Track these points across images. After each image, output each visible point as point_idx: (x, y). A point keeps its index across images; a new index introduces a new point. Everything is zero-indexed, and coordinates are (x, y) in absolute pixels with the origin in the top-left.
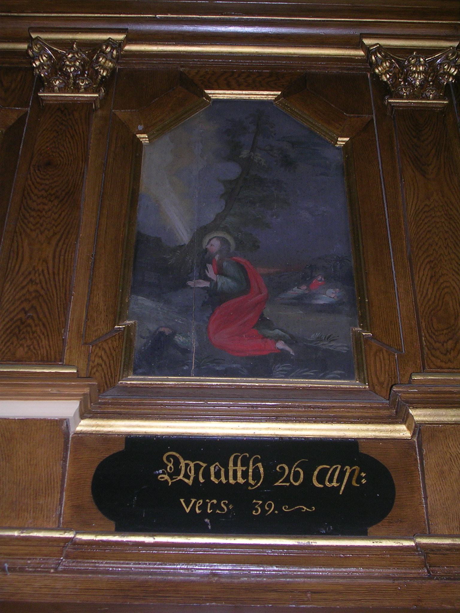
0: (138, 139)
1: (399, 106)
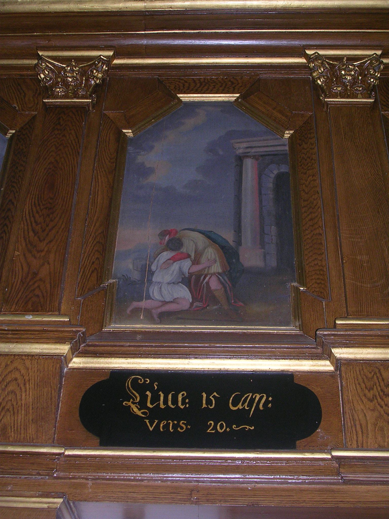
1: (336, 104)
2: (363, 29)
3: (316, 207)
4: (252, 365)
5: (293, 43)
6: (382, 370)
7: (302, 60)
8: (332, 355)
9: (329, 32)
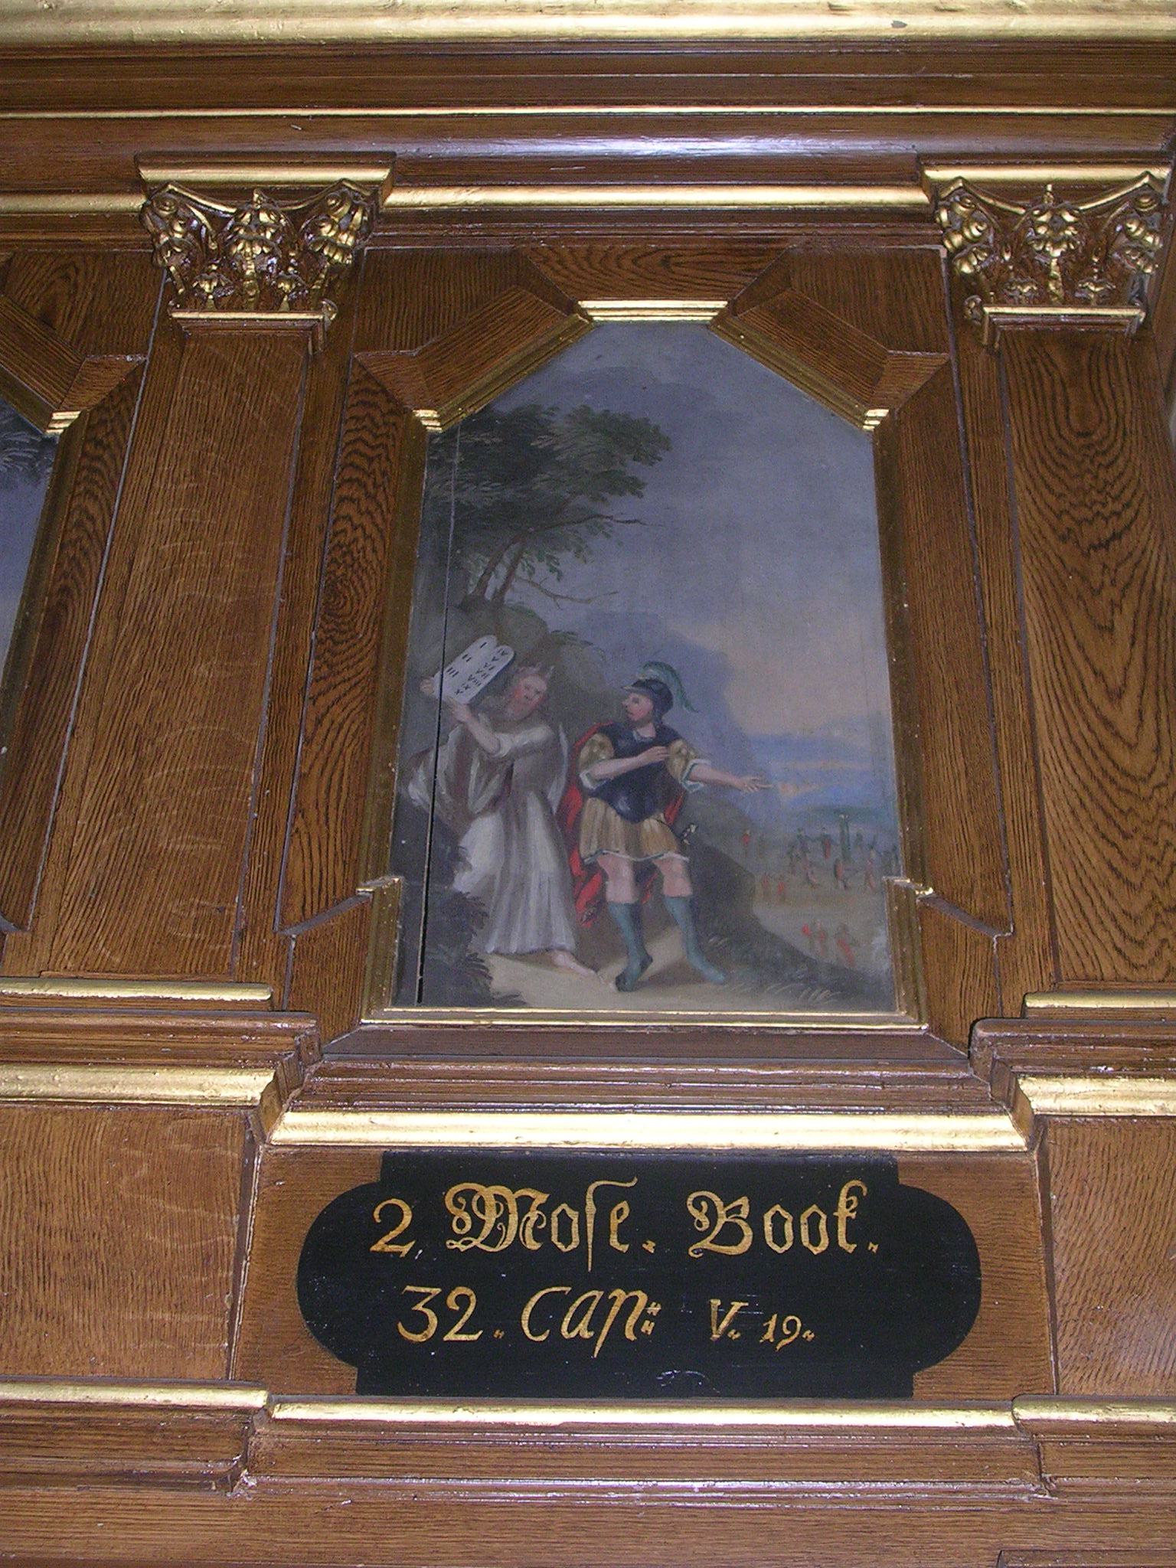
0: (418, 420)
1: (1015, 322)
5: (690, 145)
7: (919, 197)
8: (1020, 1099)
9: (549, 104)
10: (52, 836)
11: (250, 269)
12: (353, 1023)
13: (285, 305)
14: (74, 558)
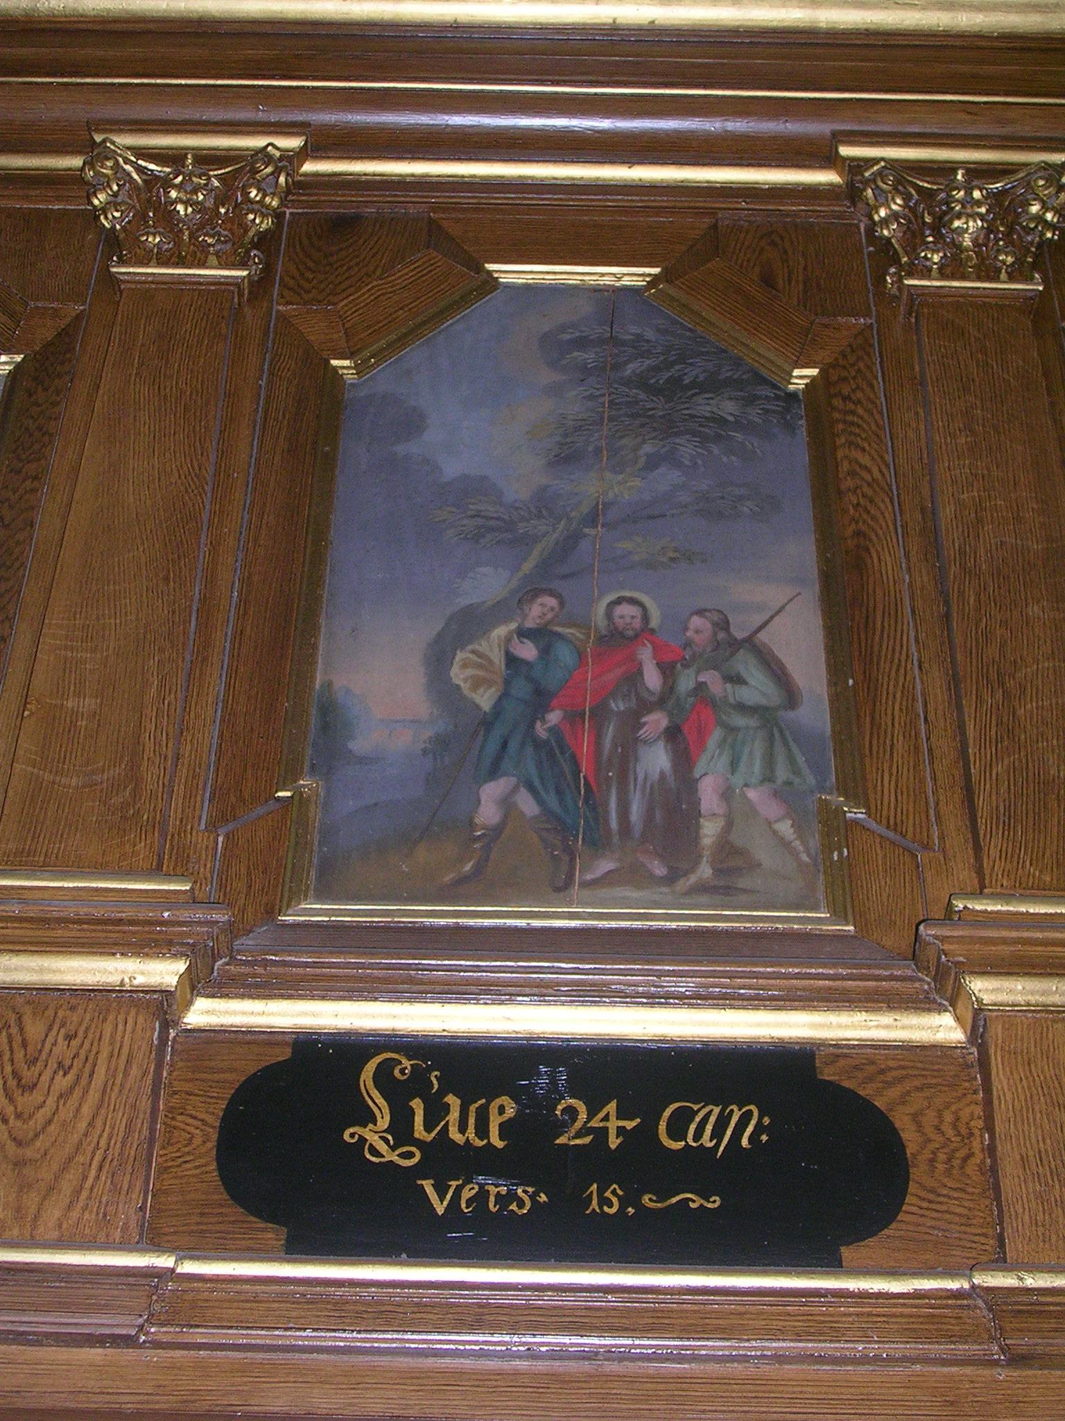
2: (222, 77)
3: (17, 565)
4: (388, 1016)
6: (27, 1020)
10: (932, 762)
11: (967, 241)
12: (274, 919)
13: (1003, 275)
14: (858, 504)
